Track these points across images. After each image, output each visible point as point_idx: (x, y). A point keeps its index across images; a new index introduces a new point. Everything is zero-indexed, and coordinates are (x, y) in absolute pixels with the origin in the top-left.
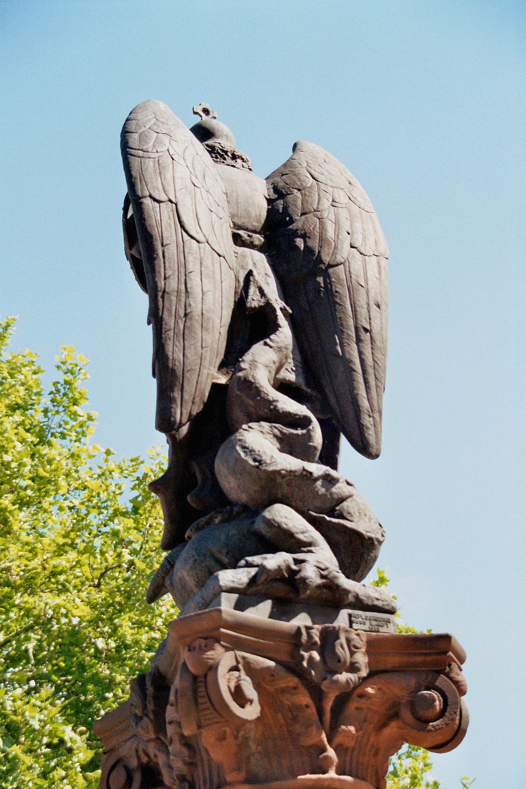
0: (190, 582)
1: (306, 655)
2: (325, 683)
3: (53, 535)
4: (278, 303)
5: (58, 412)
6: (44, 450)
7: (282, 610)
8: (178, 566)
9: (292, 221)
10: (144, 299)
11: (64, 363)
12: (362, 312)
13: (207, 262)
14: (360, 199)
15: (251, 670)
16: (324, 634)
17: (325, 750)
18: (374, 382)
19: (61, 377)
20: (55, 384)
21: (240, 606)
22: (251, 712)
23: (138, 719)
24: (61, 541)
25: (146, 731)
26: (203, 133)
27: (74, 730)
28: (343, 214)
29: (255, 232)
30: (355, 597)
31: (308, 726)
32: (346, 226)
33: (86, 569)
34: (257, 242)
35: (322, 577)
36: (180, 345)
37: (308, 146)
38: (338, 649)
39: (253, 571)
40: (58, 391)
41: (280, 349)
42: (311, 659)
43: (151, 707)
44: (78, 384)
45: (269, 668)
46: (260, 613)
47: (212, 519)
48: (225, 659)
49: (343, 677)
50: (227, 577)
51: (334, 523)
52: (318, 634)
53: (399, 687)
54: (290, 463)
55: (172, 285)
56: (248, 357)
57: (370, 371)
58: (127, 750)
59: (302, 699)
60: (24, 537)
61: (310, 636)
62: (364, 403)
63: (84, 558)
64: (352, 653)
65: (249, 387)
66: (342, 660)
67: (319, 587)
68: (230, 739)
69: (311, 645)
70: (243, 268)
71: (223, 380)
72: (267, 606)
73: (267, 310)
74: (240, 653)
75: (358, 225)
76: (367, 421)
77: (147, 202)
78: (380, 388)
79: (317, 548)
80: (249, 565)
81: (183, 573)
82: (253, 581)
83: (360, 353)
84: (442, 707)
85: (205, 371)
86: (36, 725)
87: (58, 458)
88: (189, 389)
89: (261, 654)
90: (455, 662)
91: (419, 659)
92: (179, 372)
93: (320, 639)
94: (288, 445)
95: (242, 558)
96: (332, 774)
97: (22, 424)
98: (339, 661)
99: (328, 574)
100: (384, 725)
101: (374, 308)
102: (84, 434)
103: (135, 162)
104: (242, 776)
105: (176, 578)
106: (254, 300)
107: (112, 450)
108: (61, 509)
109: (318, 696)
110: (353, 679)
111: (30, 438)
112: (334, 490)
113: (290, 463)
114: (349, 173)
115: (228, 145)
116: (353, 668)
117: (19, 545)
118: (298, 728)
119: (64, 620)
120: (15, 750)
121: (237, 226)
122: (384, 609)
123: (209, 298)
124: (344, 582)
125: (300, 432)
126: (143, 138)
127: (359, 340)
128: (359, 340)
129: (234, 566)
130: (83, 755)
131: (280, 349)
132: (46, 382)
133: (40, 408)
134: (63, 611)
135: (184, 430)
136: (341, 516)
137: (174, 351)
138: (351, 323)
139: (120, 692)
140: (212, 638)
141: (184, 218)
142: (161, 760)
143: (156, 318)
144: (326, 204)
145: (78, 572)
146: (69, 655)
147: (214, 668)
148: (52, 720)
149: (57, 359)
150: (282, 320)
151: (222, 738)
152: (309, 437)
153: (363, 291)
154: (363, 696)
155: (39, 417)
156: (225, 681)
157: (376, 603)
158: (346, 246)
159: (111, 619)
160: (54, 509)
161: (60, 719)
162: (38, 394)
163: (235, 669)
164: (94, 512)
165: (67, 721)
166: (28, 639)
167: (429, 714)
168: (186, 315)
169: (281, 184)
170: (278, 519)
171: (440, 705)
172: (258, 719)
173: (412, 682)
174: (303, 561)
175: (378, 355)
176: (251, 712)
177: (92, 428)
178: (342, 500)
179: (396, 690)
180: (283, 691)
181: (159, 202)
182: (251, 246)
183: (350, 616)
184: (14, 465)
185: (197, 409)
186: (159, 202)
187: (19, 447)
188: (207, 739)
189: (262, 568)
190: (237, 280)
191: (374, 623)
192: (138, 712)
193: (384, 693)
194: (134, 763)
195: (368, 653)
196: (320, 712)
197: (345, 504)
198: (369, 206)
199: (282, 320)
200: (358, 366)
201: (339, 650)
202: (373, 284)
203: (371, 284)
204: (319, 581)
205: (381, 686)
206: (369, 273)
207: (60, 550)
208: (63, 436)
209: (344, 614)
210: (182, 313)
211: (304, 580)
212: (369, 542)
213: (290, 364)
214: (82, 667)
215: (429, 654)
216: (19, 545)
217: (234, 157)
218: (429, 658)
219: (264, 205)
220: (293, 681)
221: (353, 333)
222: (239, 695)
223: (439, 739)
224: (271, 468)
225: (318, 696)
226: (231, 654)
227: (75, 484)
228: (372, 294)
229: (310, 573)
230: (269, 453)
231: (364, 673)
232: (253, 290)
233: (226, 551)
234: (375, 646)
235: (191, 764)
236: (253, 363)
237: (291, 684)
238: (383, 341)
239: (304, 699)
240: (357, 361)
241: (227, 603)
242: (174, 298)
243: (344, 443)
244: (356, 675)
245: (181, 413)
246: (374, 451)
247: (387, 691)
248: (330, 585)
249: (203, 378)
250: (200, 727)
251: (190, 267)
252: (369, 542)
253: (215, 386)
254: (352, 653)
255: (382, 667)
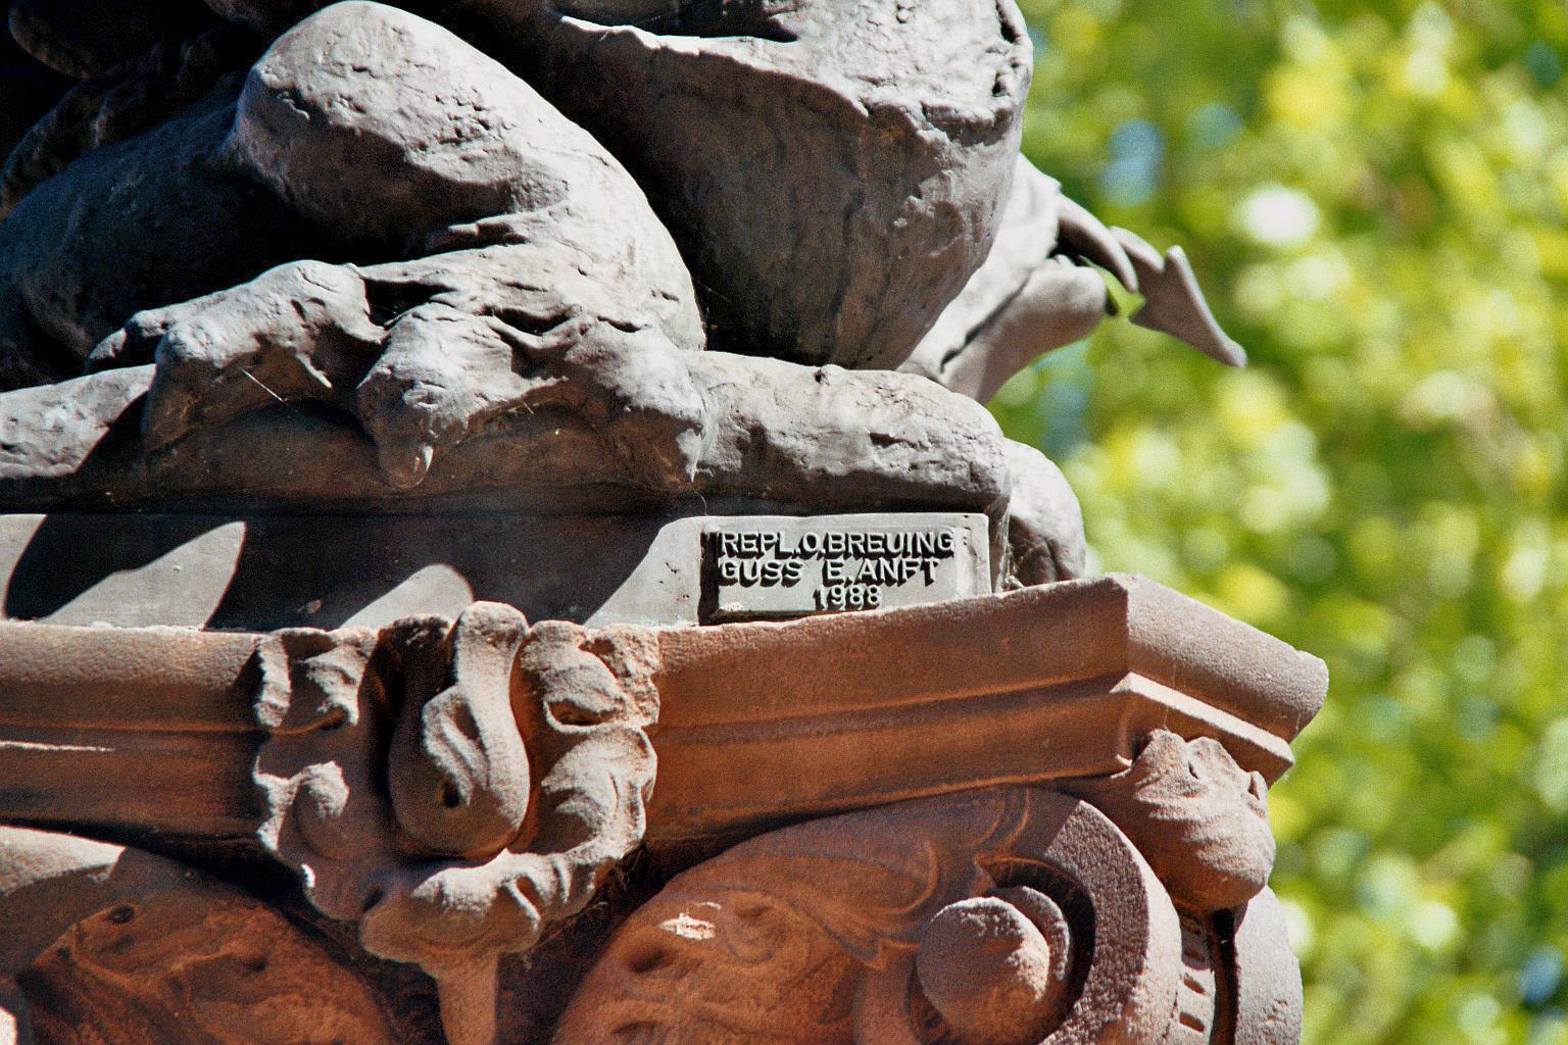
2: (373, 919)
30: (740, 443)
35: (526, 362)
38: (441, 737)
42: (304, 801)
45: (80, 880)
47: (75, 119)
51: (686, 58)
52: (356, 671)
59: (300, 1015)
64: (545, 751)
66: (465, 790)
79: (541, 213)
84: (1061, 974)
89: (16, 814)
90: (1191, 728)
93: (366, 695)
98: (452, 798)
99: (562, 349)
110: (543, 881)
122: (918, 486)
157: (876, 459)
171: (1054, 960)
179: (836, 911)
183: (711, 545)
191: (850, 569)
193: (780, 934)
204: (506, 386)
205: (755, 899)
212: (887, 138)
215: (1018, 699)
218: (1023, 722)
233: (76, 289)
237: (236, 947)
244: (561, 861)
247: (793, 917)
252: (887, 138)
255: (774, 801)
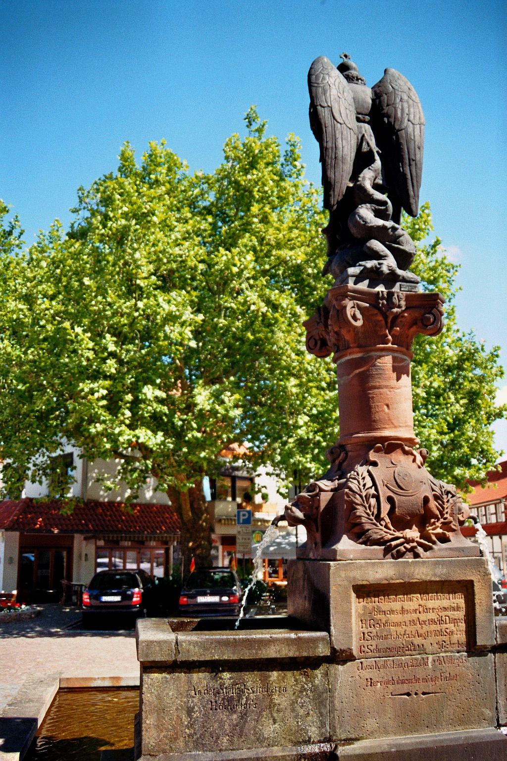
0: (338, 271)
1: (381, 302)
3: (287, 223)
4: (375, 149)
5: (288, 165)
6: (283, 184)
7: (372, 285)
8: (333, 264)
9: (383, 109)
10: (317, 144)
11: (290, 141)
12: (412, 152)
13: (345, 133)
14: (413, 97)
15: (359, 307)
16: (388, 293)
17: (387, 336)
18: (416, 184)
19: (289, 148)
20: (286, 151)
21: (356, 283)
22: (359, 323)
23: (318, 323)
24: (291, 225)
25: (321, 327)
26: (343, 68)
27: (301, 307)
28: (405, 105)
29: (366, 115)
31: (381, 328)
32: (406, 111)
33: (303, 238)
34: (367, 120)
36: (333, 171)
37: (392, 71)
39: (362, 268)
40: (287, 155)
41: (375, 171)
42: (383, 303)
43: (323, 319)
44: (296, 151)
45: (366, 307)
46: (363, 286)
48: (349, 304)
49: (395, 310)
50: (352, 270)
53: (416, 314)
54: (380, 222)
55: (330, 145)
56: (361, 175)
57: (415, 178)
58: (315, 333)
60: (275, 225)
61: (383, 295)
62: (411, 193)
63: (302, 233)
64: (399, 301)
65: (363, 189)
67: (388, 274)
68: (352, 332)
69: (383, 298)
70: (360, 133)
71: (351, 185)
72: (367, 282)
73: (371, 152)
74: (355, 301)
75: (412, 110)
76: (412, 201)
77: (319, 108)
78: (419, 186)
80: (360, 265)
81: (334, 266)
82: (362, 272)
83: (410, 171)
85: (343, 182)
86: (285, 306)
87: (288, 187)
88: (337, 190)
91: (426, 302)
92: (333, 183)
94: (379, 214)
95: (358, 262)
96: (390, 345)
97: (272, 171)
100: (411, 327)
101: (417, 150)
102: (300, 175)
103: (314, 89)
104: (356, 345)
105: (333, 268)
106: (365, 148)
107: (313, 183)
108: (291, 211)
109: (385, 317)
111: (276, 178)
112: (396, 233)
113: (380, 222)
114: (409, 83)
115: (353, 73)
116: (399, 307)
117: (273, 229)
118: (378, 328)
119: (294, 262)
120: (277, 315)
121: (358, 113)
123: (345, 149)
124: (400, 272)
125: (383, 208)
126: (317, 77)
127: (410, 165)
128: (410, 165)
129: (354, 266)
130: (304, 318)
131: (375, 171)
132: (283, 149)
133: (279, 163)
134: (293, 257)
135: (335, 207)
136: (399, 243)
137: (330, 174)
138: (407, 156)
139: (319, 292)
140: (345, 296)
141: (335, 113)
142: (327, 337)
143: (323, 159)
144: (398, 100)
145: (299, 239)
146: (297, 276)
147: (345, 307)
148: (291, 304)
149: (287, 140)
150: (377, 157)
151: (349, 331)
152: (386, 210)
153: (413, 142)
154: (403, 316)
155: (279, 167)
156: (349, 312)
158: (406, 120)
159: (314, 261)
160: (288, 211)
161: (295, 304)
162: (279, 157)
163: (353, 307)
164: (305, 213)
165: (297, 304)
166: (279, 269)
167: (428, 323)
168: (335, 158)
169: (378, 91)
170: (373, 246)
172: (362, 325)
173: (423, 311)
174: (382, 264)
175: (418, 171)
176: (359, 323)
177: (303, 172)
178: (400, 236)
179: (416, 315)
180: (372, 315)
181: (324, 107)
182: (364, 122)
184: (269, 192)
185: (340, 198)
186: (324, 107)
187: (271, 182)
188: (343, 332)
189: (365, 267)
190: (358, 139)
192: (318, 321)
194: (317, 338)
195: (406, 300)
196: (386, 323)
197: (401, 238)
198: (417, 100)
199: (377, 157)
200: (409, 176)
201: (394, 300)
202: (417, 138)
203: (416, 138)
204: (388, 272)
206: (416, 133)
207: (290, 229)
208: (290, 176)
209: (398, 284)
210: (334, 157)
211: (382, 271)
213: (380, 177)
214: (303, 280)
216: (273, 229)
217: (358, 79)
219: (370, 101)
220: (376, 311)
221: (407, 162)
222: (354, 317)
223: (432, 332)
224: (370, 225)
225: (385, 317)
226: (352, 302)
227: (296, 199)
228: (417, 143)
229: (385, 269)
230: (369, 217)
231: (403, 308)
232: (364, 143)
234: (408, 298)
235: (338, 340)
236: (364, 178)
238: (421, 164)
239: (380, 318)
240: (409, 174)
241: (351, 284)
242: (330, 151)
243: (403, 212)
245: (335, 199)
246: (415, 214)
248: (392, 272)
249: (343, 185)
250: (340, 328)
251: (337, 136)
253: (348, 187)
254: (399, 301)
